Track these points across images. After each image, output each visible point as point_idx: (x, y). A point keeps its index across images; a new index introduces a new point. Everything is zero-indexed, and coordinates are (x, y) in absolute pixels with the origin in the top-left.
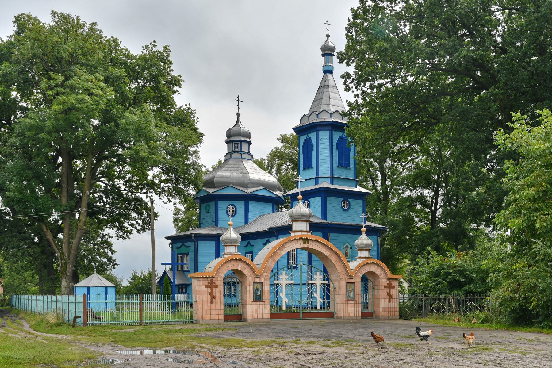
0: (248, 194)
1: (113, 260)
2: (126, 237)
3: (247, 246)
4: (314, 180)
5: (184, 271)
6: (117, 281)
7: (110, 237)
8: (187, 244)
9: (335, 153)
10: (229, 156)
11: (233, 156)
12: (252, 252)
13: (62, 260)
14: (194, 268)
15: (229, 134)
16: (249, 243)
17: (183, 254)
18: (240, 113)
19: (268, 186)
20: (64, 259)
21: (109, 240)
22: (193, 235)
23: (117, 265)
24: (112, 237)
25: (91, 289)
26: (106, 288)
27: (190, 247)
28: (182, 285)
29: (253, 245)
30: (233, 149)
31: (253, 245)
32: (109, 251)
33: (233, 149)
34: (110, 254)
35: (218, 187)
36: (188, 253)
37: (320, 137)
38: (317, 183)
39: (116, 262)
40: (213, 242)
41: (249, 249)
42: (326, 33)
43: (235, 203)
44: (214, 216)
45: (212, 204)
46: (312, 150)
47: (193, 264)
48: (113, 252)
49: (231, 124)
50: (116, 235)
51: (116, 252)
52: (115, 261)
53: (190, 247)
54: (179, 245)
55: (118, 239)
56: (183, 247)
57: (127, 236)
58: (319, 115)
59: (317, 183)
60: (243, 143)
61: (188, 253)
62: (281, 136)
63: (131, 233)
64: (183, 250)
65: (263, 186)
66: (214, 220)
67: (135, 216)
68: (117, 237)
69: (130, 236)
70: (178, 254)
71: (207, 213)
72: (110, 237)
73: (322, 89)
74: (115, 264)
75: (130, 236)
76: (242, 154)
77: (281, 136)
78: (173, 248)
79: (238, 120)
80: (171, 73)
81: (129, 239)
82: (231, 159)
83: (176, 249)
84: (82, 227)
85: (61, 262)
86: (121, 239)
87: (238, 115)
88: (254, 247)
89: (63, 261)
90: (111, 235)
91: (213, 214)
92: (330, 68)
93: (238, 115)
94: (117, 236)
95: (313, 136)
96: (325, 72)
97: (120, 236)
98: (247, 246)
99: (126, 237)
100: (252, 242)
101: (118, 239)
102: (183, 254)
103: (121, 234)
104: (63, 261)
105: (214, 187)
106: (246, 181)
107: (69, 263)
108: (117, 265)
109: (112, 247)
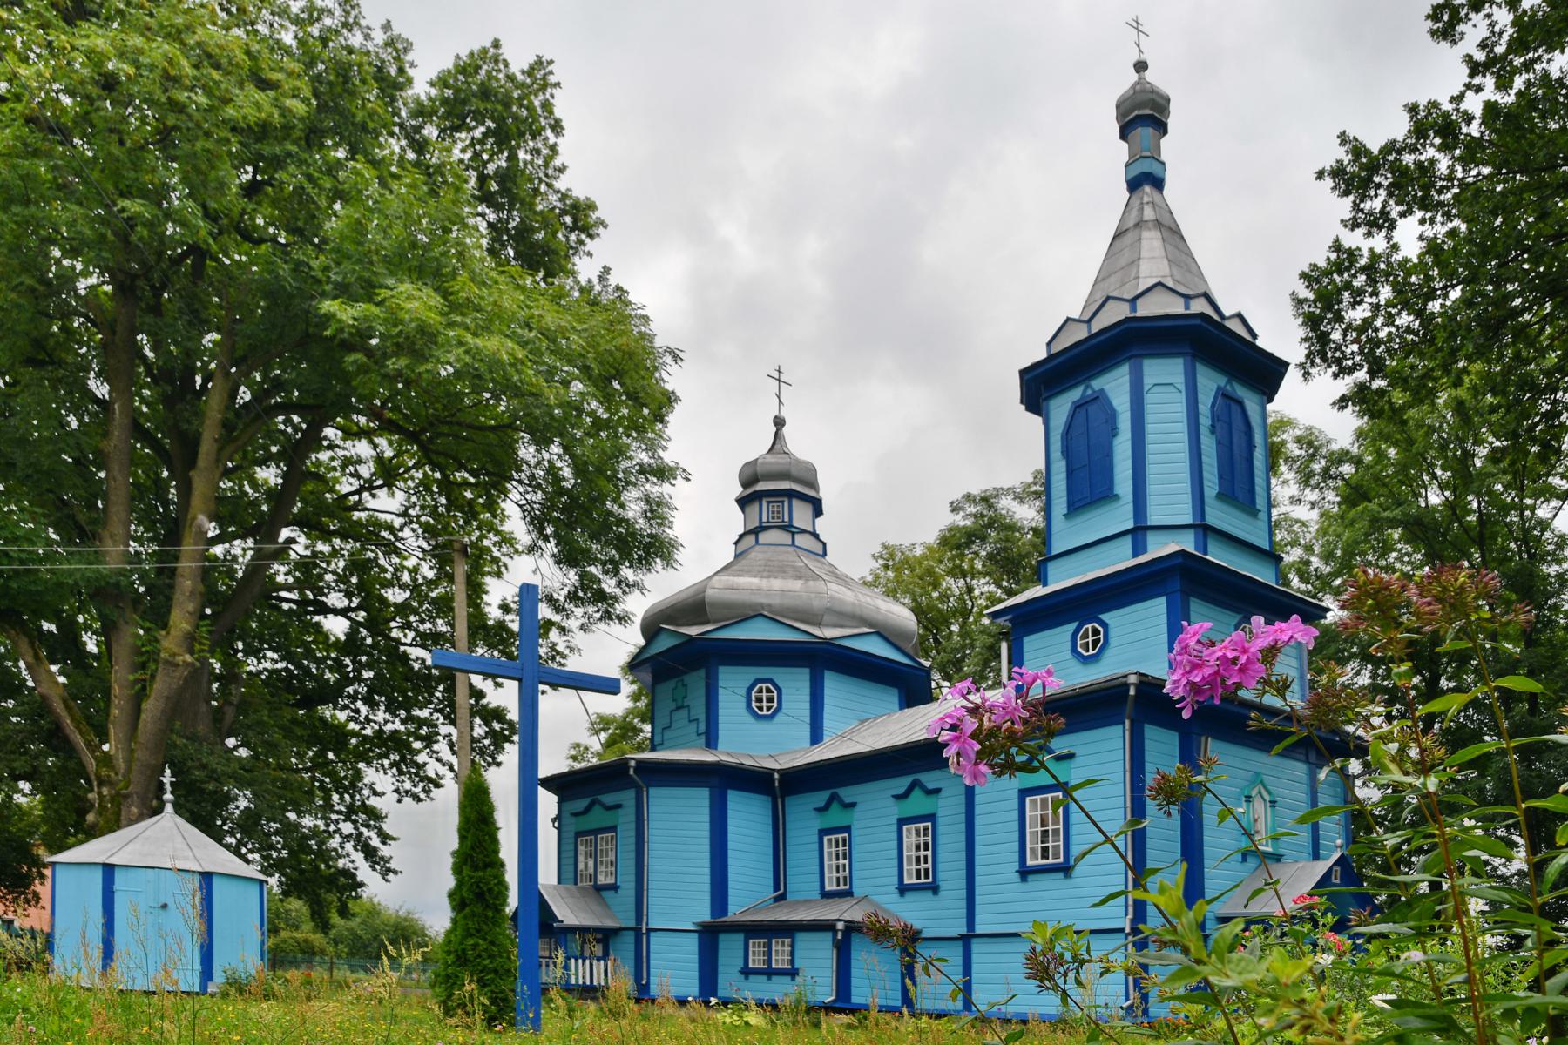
0: (828, 642)
1: (382, 858)
2: (422, 795)
3: (826, 808)
4: (1128, 540)
5: (599, 889)
6: (426, 935)
7: (375, 793)
8: (608, 799)
9: (1208, 444)
10: (751, 539)
11: (765, 537)
12: (847, 829)
13: (101, 784)
14: (633, 878)
15: (750, 476)
16: (833, 798)
17: (596, 832)
18: (784, 414)
19: (885, 633)
20: (111, 784)
21: (374, 801)
22: (633, 763)
23: (395, 872)
24: (384, 794)
25: (119, 876)
26: (207, 877)
27: (619, 806)
28: (596, 930)
29: (853, 805)
30: (765, 519)
31: (853, 805)
32: (374, 837)
33: (765, 519)
34: (375, 842)
35: (715, 622)
36: (613, 829)
37: (1148, 381)
38: (1138, 549)
39: (392, 865)
40: (704, 794)
41: (836, 817)
42: (1135, 58)
43: (779, 674)
44: (702, 718)
45: (696, 680)
46: (1114, 431)
47: (633, 862)
48: (385, 838)
49: (756, 446)
50: (394, 788)
51: (395, 839)
52: (388, 861)
53: (619, 806)
54: (581, 804)
55: (399, 801)
56: (597, 809)
57: (427, 791)
58: (1139, 302)
59: (1138, 549)
60: (795, 502)
61: (613, 829)
62: (885, 546)
63: (438, 786)
64: (597, 818)
65: (871, 626)
66: (702, 728)
67: (450, 735)
68: (396, 795)
69: (435, 792)
70: (578, 834)
71: (678, 708)
72: (375, 793)
73: (1128, 239)
74: (389, 870)
75: (435, 792)
76: (793, 534)
77: (885, 546)
78: (564, 829)
79: (777, 436)
80: (561, 184)
81: (432, 799)
82: (757, 548)
83: (573, 820)
84: (174, 655)
85: (100, 793)
86: (407, 800)
87: (779, 422)
88: (857, 808)
89: (105, 791)
90: (379, 788)
91: (699, 711)
92: (1153, 168)
93: (779, 422)
94: (397, 791)
95: (1115, 385)
96: (1134, 185)
97: (407, 792)
98: (822, 810)
99: (422, 795)
100: (847, 794)
101: (399, 801)
102: (596, 832)
103: (408, 785)
104: (105, 791)
105: (706, 622)
106: (817, 604)
107: (126, 797)
108: (395, 872)
109: (383, 825)
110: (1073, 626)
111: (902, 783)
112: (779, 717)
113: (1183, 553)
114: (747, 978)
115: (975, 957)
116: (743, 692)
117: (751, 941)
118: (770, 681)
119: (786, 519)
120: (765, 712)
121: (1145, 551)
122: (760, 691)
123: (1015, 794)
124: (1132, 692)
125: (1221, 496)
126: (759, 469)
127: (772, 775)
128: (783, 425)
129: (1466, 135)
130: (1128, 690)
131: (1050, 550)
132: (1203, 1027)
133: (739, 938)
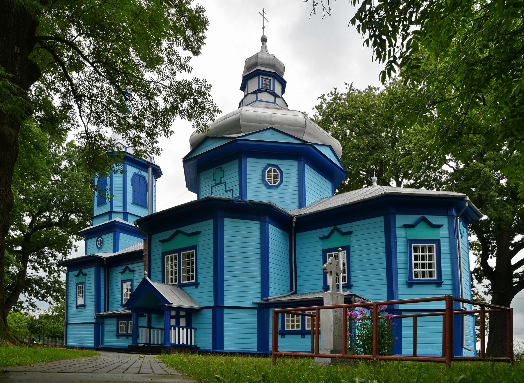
43: (281, 163)
87: (264, 40)
93: (264, 40)
100: (345, 227)
110: (96, 239)
111: (325, 231)
112: (281, 187)
113: (208, 197)
114: (118, 338)
115: (418, 323)
116: (260, 173)
117: (120, 322)
118: (276, 166)
119: (272, 89)
120: (273, 184)
121: (111, 219)
122: (270, 171)
123: (321, 253)
124: (294, 225)
125: (134, 203)
126: (260, 61)
127: (103, 259)
128: (266, 42)
129: (69, 157)
130: (293, 224)
131: (93, 214)
132: (343, 377)
133: (114, 322)
